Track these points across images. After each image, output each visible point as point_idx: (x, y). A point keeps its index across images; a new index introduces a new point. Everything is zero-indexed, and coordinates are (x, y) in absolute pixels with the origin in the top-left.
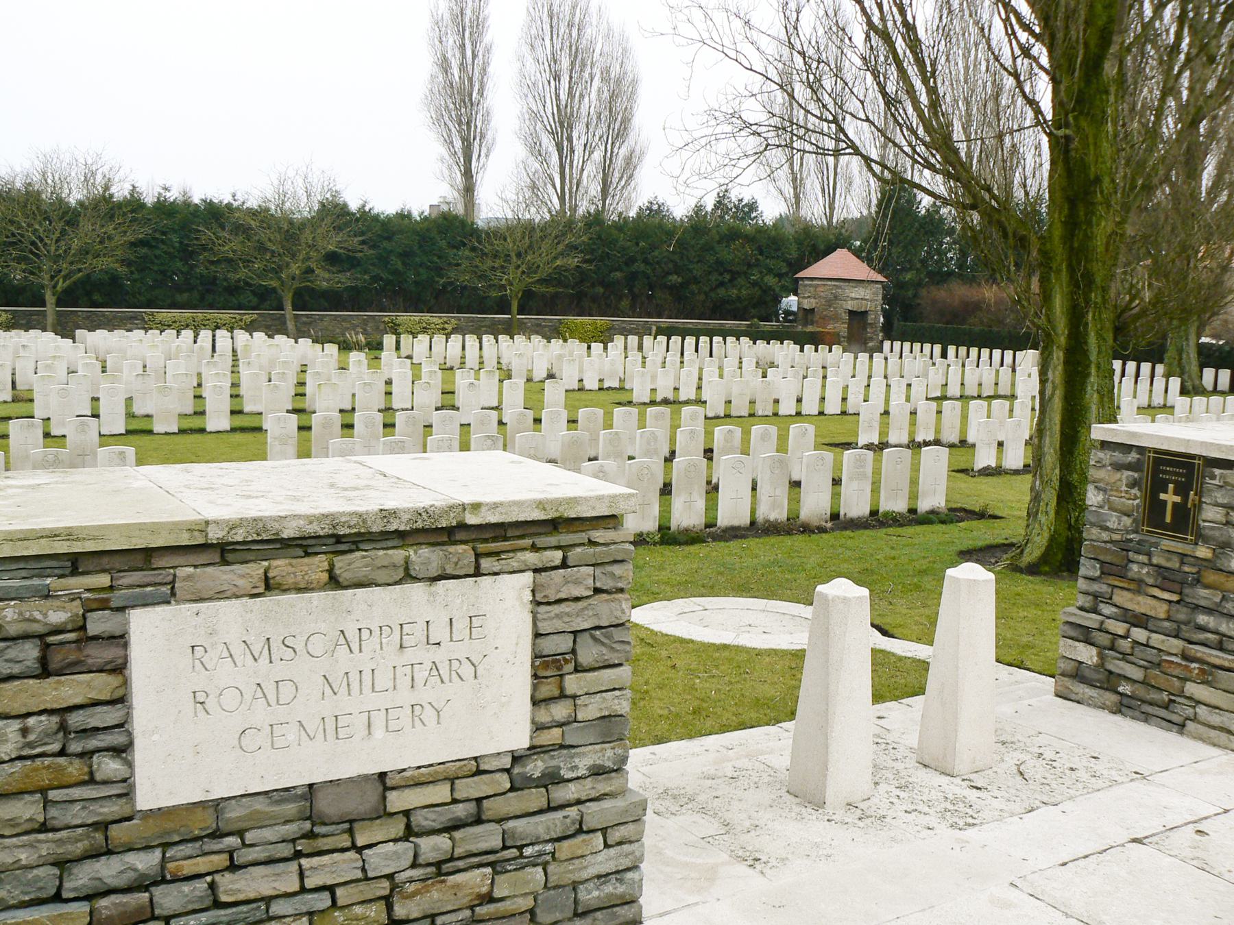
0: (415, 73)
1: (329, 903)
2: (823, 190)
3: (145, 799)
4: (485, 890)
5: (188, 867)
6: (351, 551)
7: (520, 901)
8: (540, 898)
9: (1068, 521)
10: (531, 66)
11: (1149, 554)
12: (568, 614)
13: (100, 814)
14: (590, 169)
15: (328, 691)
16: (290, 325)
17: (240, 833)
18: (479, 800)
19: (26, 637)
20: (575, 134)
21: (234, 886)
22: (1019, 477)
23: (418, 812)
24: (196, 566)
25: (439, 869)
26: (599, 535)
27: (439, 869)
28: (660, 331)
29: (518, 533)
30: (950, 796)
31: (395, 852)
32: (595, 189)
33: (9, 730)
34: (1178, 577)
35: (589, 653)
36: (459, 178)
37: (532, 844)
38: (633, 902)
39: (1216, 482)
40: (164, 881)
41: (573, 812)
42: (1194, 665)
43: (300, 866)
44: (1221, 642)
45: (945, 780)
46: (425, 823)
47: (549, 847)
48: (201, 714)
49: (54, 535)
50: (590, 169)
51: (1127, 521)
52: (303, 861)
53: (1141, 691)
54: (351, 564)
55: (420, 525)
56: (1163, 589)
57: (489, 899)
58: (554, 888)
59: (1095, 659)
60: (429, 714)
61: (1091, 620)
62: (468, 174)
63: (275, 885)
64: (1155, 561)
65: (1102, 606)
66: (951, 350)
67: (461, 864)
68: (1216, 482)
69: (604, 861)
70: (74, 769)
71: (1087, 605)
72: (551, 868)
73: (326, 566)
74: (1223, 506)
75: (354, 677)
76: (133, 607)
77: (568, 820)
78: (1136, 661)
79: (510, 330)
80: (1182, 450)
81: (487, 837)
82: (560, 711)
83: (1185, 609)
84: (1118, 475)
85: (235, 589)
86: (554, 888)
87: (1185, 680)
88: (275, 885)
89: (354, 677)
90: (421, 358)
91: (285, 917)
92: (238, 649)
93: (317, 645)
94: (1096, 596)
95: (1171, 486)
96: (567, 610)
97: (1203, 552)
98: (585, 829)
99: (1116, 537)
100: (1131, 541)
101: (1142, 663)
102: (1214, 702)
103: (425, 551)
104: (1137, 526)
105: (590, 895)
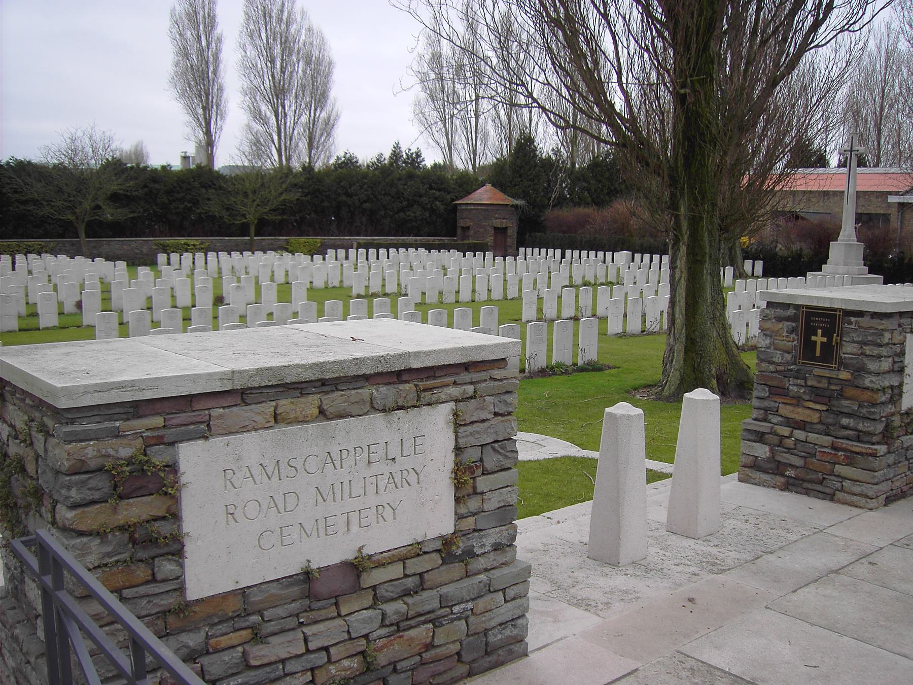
0: (163, 56)
1: (326, 659)
2: (467, 140)
3: (194, 592)
4: (429, 640)
5: (225, 641)
6: (333, 391)
7: (451, 646)
8: (464, 643)
9: (694, 366)
10: (251, 52)
11: (805, 379)
12: (478, 432)
13: (162, 605)
14: (299, 129)
15: (320, 498)
16: (84, 249)
17: (260, 612)
18: (421, 575)
19: (100, 469)
20: (287, 103)
21: (260, 654)
22: (636, 339)
23: (382, 586)
24: (224, 408)
25: (398, 626)
26: (497, 374)
27: (398, 626)
28: (359, 246)
29: (442, 374)
30: (699, 552)
31: (370, 617)
32: (303, 145)
33: (92, 544)
34: (827, 393)
35: (491, 461)
36: (201, 135)
37: (459, 604)
38: (522, 641)
39: (853, 326)
40: (208, 653)
41: (482, 577)
42: (840, 453)
43: (303, 633)
44: (859, 436)
45: (691, 542)
46: (386, 594)
47: (470, 605)
48: (232, 522)
49: (121, 386)
50: (299, 129)
51: (788, 357)
52: (306, 630)
53: (802, 474)
54: (335, 400)
55: (380, 369)
56: (814, 402)
57: (429, 646)
58: (472, 635)
59: (768, 454)
60: (388, 512)
61: (764, 427)
62: (208, 133)
63: (289, 649)
64: (809, 383)
65: (770, 417)
66: (568, 253)
67: (412, 622)
68: (853, 326)
69: (505, 612)
70: (142, 572)
71: (760, 417)
72: (472, 619)
73: (317, 403)
74: (858, 342)
75: (337, 486)
76: (181, 442)
77: (482, 585)
78: (799, 453)
79: (251, 248)
80: (827, 305)
81: (428, 600)
82: (473, 504)
83: (832, 415)
84: (780, 325)
85: (254, 424)
86: (472, 635)
87: (835, 464)
88: (289, 649)
89: (337, 486)
90: (185, 272)
91: (295, 673)
92: (257, 471)
93: (312, 465)
94: (766, 410)
95: (820, 331)
96: (478, 429)
97: (844, 375)
98: (492, 589)
99: (779, 368)
100: (791, 370)
101: (803, 454)
102: (855, 478)
103: (383, 389)
104: (795, 360)
105: (495, 638)
